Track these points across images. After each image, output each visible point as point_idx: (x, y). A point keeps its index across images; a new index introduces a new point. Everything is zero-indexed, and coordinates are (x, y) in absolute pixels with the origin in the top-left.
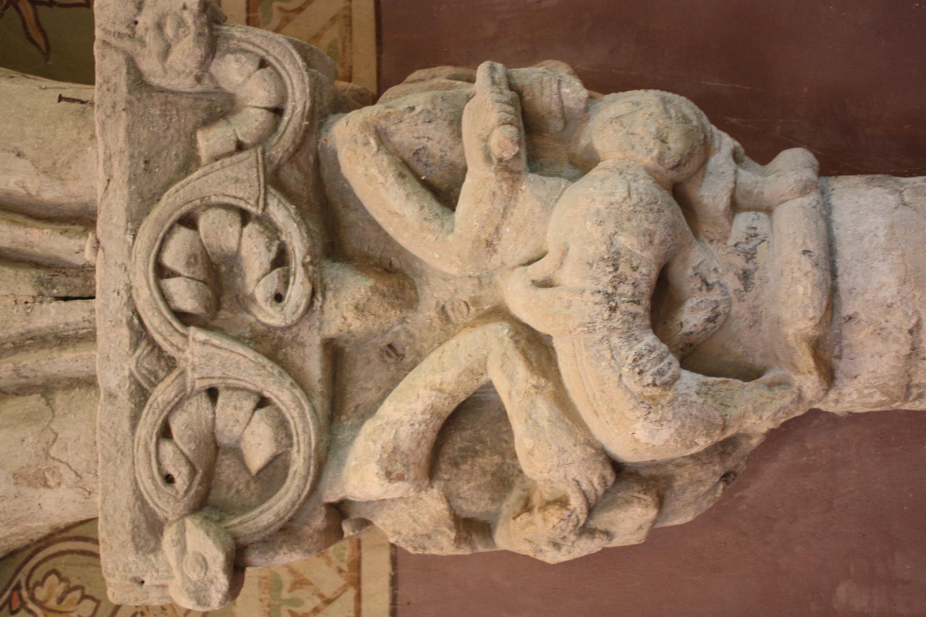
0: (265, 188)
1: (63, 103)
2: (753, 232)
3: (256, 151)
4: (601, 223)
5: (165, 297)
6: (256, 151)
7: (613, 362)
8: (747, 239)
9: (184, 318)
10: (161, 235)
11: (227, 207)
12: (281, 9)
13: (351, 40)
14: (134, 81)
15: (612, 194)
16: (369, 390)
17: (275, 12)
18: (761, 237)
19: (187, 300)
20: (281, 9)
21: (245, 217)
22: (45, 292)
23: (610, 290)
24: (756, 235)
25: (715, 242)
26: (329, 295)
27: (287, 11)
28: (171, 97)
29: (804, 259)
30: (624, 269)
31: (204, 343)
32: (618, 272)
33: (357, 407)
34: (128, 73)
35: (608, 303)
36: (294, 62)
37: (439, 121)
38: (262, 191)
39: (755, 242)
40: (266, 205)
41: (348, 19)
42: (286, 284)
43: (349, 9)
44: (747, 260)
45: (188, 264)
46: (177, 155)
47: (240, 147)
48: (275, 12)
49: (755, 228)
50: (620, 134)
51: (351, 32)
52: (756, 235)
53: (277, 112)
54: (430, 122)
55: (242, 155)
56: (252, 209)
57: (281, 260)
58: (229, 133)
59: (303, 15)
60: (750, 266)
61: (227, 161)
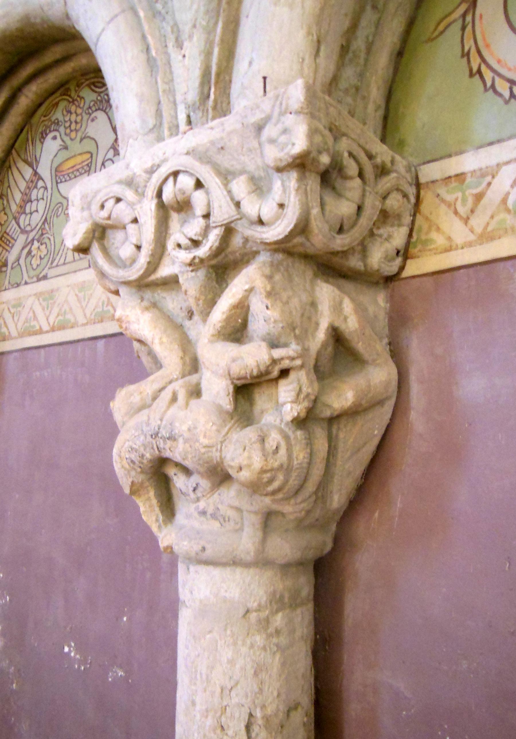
0: (221, 226)
1: (262, 80)
2: (227, 519)
3: (236, 215)
4: (189, 430)
5: (166, 179)
6: (236, 215)
7: (133, 436)
8: (222, 515)
9: (159, 194)
10: (188, 170)
11: (209, 205)
12: (457, 199)
13: (435, 254)
14: (259, 125)
15: (205, 436)
16: (173, 304)
17: (454, 196)
18: (224, 524)
19: (168, 194)
20: (457, 199)
21: (207, 216)
22: (191, 109)
23: (160, 435)
24: (225, 521)
25: (219, 496)
26: (193, 274)
27: (455, 204)
28: (258, 151)
29: (200, 547)
30: (169, 443)
31: (151, 210)
32: (167, 440)
33: (165, 298)
34: (262, 119)
35: (154, 434)
36: (287, 226)
37: (267, 327)
38: (220, 224)
39: (222, 520)
40: (216, 227)
41: (448, 250)
42: (186, 249)
43: (457, 248)
44: (211, 515)
45: (180, 190)
46: (232, 166)
47: (238, 205)
48: (454, 196)
49: (229, 521)
50: (247, 441)
51: (441, 253)
52: (225, 521)
53: (261, 222)
54: (265, 321)
55: (233, 207)
56: (212, 219)
57: (196, 243)
58: (242, 195)
59: (453, 215)
60: (209, 516)
61: (228, 199)
